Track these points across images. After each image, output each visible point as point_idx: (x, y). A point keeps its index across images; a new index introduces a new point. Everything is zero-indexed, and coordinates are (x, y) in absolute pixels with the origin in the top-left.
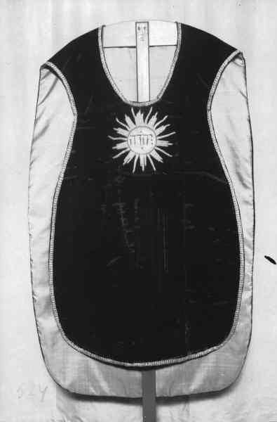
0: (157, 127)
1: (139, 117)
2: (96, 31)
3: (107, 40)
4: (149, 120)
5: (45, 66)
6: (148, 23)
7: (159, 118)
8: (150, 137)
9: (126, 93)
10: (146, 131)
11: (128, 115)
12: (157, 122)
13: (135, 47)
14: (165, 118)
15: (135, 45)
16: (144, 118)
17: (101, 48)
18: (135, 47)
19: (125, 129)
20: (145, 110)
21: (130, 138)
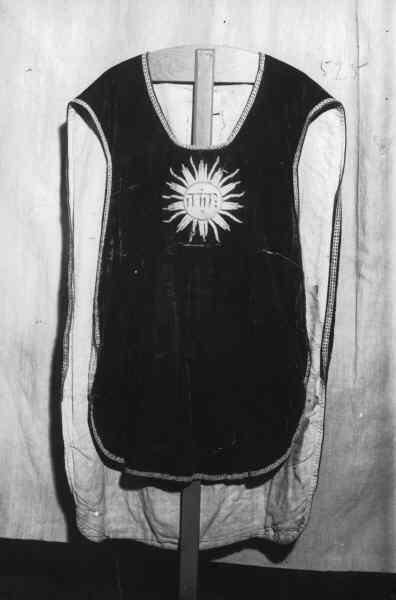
0: (225, 184)
1: (203, 168)
2: (138, 60)
3: (151, 72)
4: (212, 176)
5: (73, 105)
6: (213, 50)
7: (198, 236)
8: (213, 197)
9: (181, 136)
10: (208, 189)
11: (170, 182)
12: (222, 179)
13: (216, 84)
14: (118, 459)
15: (192, 80)
16: (208, 172)
17: (257, 86)
18: (216, 84)
19: (193, 174)
20: (208, 157)
21: (187, 196)
